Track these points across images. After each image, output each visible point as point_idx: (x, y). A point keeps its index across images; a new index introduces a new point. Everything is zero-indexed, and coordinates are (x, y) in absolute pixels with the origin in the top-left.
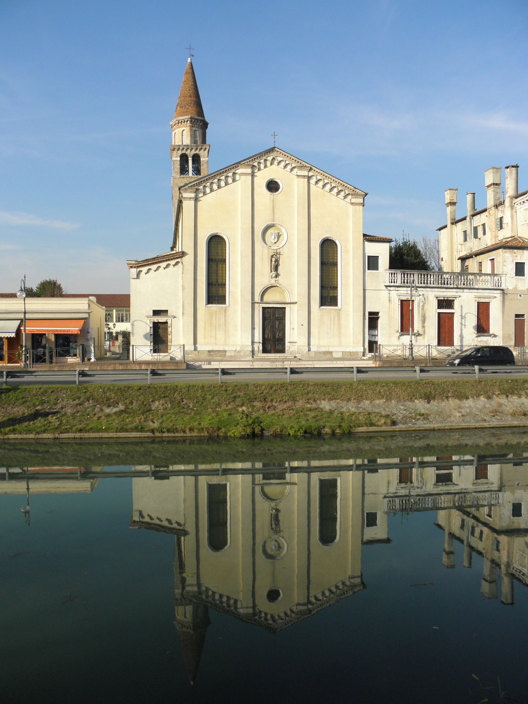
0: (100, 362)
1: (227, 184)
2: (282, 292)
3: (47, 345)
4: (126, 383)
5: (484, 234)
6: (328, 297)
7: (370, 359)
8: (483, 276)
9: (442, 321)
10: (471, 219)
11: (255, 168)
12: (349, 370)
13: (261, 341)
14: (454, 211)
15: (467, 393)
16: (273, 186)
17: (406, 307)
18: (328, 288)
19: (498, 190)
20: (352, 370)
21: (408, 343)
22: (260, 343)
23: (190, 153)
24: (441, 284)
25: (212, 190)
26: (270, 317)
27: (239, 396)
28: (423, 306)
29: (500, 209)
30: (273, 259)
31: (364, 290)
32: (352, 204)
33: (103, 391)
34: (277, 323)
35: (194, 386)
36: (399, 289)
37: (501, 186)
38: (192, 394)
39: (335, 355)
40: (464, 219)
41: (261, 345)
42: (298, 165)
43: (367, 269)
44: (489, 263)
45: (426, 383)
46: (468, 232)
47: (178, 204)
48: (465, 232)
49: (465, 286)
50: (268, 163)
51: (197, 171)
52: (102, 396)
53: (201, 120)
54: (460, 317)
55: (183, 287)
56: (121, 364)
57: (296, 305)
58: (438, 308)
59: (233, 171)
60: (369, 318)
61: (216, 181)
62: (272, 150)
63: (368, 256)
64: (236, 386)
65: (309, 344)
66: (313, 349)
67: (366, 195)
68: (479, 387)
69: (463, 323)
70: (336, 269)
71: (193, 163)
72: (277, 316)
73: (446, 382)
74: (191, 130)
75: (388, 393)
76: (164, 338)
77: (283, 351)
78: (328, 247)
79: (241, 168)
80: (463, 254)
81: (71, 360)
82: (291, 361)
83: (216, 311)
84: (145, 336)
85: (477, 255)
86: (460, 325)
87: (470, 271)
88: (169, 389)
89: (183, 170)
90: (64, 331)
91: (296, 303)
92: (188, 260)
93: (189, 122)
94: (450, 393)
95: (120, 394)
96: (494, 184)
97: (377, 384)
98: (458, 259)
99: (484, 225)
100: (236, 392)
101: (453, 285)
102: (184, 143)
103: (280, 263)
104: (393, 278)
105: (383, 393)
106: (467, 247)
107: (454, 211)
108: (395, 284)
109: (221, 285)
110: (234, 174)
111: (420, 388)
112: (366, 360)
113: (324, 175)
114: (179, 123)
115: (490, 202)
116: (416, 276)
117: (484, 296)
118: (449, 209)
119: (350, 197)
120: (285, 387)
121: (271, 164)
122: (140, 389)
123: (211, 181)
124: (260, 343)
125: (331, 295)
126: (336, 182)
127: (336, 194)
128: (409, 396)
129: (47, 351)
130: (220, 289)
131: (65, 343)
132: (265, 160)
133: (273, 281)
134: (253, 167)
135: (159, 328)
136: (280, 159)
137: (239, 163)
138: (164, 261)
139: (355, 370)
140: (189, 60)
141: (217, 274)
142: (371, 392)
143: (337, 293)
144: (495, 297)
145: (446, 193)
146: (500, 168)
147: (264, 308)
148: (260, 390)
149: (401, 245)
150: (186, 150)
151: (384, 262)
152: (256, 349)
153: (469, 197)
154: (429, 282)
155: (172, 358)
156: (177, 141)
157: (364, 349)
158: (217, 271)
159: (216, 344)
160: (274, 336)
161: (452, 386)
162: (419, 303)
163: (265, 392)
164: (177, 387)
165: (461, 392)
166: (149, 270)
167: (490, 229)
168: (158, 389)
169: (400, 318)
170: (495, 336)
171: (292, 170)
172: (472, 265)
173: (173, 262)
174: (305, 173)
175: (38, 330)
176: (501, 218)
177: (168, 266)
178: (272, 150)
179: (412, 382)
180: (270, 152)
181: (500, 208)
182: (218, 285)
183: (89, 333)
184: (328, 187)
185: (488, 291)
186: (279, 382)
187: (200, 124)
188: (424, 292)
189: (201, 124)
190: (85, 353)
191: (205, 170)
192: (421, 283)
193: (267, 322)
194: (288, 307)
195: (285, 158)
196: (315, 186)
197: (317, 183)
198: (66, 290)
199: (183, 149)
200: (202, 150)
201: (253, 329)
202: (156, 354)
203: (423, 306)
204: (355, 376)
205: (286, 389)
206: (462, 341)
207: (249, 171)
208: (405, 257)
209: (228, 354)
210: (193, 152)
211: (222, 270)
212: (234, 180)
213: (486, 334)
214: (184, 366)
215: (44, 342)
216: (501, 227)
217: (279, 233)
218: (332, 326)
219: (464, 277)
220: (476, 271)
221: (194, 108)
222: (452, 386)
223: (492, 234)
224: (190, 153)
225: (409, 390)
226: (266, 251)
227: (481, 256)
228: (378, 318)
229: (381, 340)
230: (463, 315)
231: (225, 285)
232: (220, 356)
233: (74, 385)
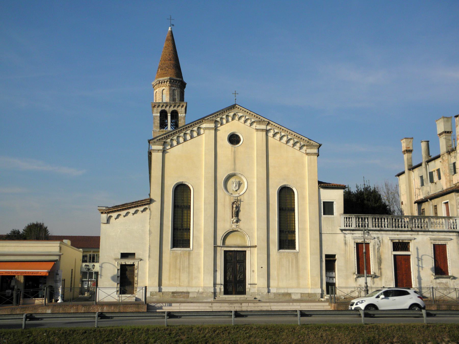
0: (66, 303)
1: (192, 137)
2: (243, 237)
3: (16, 287)
4: (74, 327)
5: (440, 178)
6: (287, 241)
7: (327, 301)
8: (440, 219)
9: (399, 263)
10: (426, 165)
11: (218, 123)
12: (293, 313)
13: (223, 283)
14: (411, 158)
15: (414, 339)
16: (234, 139)
17: (362, 251)
18: (286, 232)
19: (450, 138)
20: (296, 313)
21: (363, 285)
22: (221, 284)
23: (169, 110)
24: (396, 227)
25: (178, 143)
26: (232, 260)
27: (182, 340)
28: (379, 249)
29: (453, 155)
30: (234, 206)
31: (321, 234)
32: (307, 154)
33: (48, 335)
34: (238, 266)
35: (139, 329)
36: (354, 232)
37: (453, 134)
38: (136, 337)
39: (294, 297)
40: (420, 165)
41: (222, 287)
42: (257, 119)
44: (444, 207)
45: (370, 328)
46: (424, 177)
47: (148, 156)
48: (422, 177)
49: (420, 229)
50: (230, 119)
51: (175, 125)
52: (44, 341)
53: (179, 81)
54: (416, 259)
55: (150, 231)
56: (83, 306)
57: (256, 249)
58: (394, 250)
59: (198, 126)
60: (326, 261)
61: (182, 134)
62: (233, 107)
63: (324, 202)
64: (180, 329)
65: (268, 286)
66: (273, 290)
67: (320, 145)
68: (426, 333)
69: (420, 265)
70: (293, 214)
71: (171, 119)
72: (238, 259)
73: (391, 326)
74: (170, 90)
75: (330, 337)
76: (131, 280)
77: (243, 292)
78: (286, 194)
79: (205, 123)
80: (421, 197)
81: (38, 301)
82: (249, 303)
83: (181, 254)
84: (113, 278)
85: (432, 198)
86: (417, 267)
87: (427, 214)
88: (113, 332)
89: (163, 125)
90: (33, 273)
91: (256, 246)
92: (156, 206)
93: (168, 82)
94: (396, 338)
95: (63, 338)
96: (445, 132)
97: (320, 327)
98: (415, 203)
99: (438, 170)
100: (179, 336)
101: (408, 227)
102: (164, 101)
103: (241, 209)
104: (348, 222)
105: (325, 338)
106: (424, 192)
107: (411, 158)
108: (350, 228)
109: (186, 229)
110: (199, 128)
111: (363, 332)
112: (324, 302)
113: (280, 129)
114: (159, 83)
115: (443, 149)
116: (370, 220)
117: (440, 238)
118: (406, 156)
119: (305, 148)
120: (228, 331)
121: (233, 119)
122: (85, 332)
123: (177, 135)
124: (221, 284)
125: (289, 238)
126: (292, 134)
127: (292, 146)
128: (351, 341)
129: (14, 293)
130: (185, 233)
131: (34, 285)
132: (227, 116)
133: (234, 226)
134: (216, 122)
135: (126, 270)
136: (240, 114)
137: (203, 118)
138: (133, 207)
139: (298, 313)
140: (170, 29)
141: (182, 219)
142: (313, 336)
143: (295, 237)
144: (451, 239)
145: (402, 141)
146: (451, 118)
147: (225, 252)
148: (203, 333)
149: (362, 190)
150: (166, 107)
151: (339, 207)
152: (218, 290)
153: (423, 145)
154: (383, 225)
155: (137, 299)
156: (157, 99)
157: (322, 291)
158: (182, 216)
159: (180, 286)
160: (235, 277)
161: (397, 331)
162: (374, 246)
163: (207, 336)
164: (122, 330)
165: (407, 338)
166: (119, 215)
167: (444, 174)
168: (103, 332)
169: (356, 261)
170: (454, 278)
171: (251, 124)
172: (428, 208)
173: (141, 208)
174: (264, 127)
175: (6, 272)
176: (454, 164)
177: (136, 212)
178: (233, 107)
179: (355, 326)
180: (231, 108)
181: (452, 154)
182: (183, 230)
183: (58, 274)
184: (285, 139)
185: (443, 234)
186: (224, 325)
187: (178, 85)
188: (379, 235)
190: (52, 295)
191: (181, 123)
192: (376, 227)
193: (229, 264)
195: (245, 114)
196: (272, 139)
197: (274, 135)
198: (52, 232)
199: (163, 106)
200: (180, 107)
201: (215, 271)
202: (123, 295)
203: (379, 249)
204: (299, 320)
205: (229, 333)
206: (420, 283)
207: (213, 125)
208: (366, 202)
209: (191, 295)
210: (172, 109)
211: (187, 216)
212: (199, 134)
213: (444, 276)
214: (144, 309)
215: (13, 283)
216: (455, 172)
217: (239, 182)
219: (420, 221)
220: (432, 214)
221: (173, 70)
222: (397, 331)
223: (446, 179)
224: (169, 110)
225: (352, 334)
226: (227, 198)
227: (436, 200)
228: (335, 260)
229: (338, 281)
230: (420, 257)
231: (189, 229)
232: (183, 297)
233: (20, 330)
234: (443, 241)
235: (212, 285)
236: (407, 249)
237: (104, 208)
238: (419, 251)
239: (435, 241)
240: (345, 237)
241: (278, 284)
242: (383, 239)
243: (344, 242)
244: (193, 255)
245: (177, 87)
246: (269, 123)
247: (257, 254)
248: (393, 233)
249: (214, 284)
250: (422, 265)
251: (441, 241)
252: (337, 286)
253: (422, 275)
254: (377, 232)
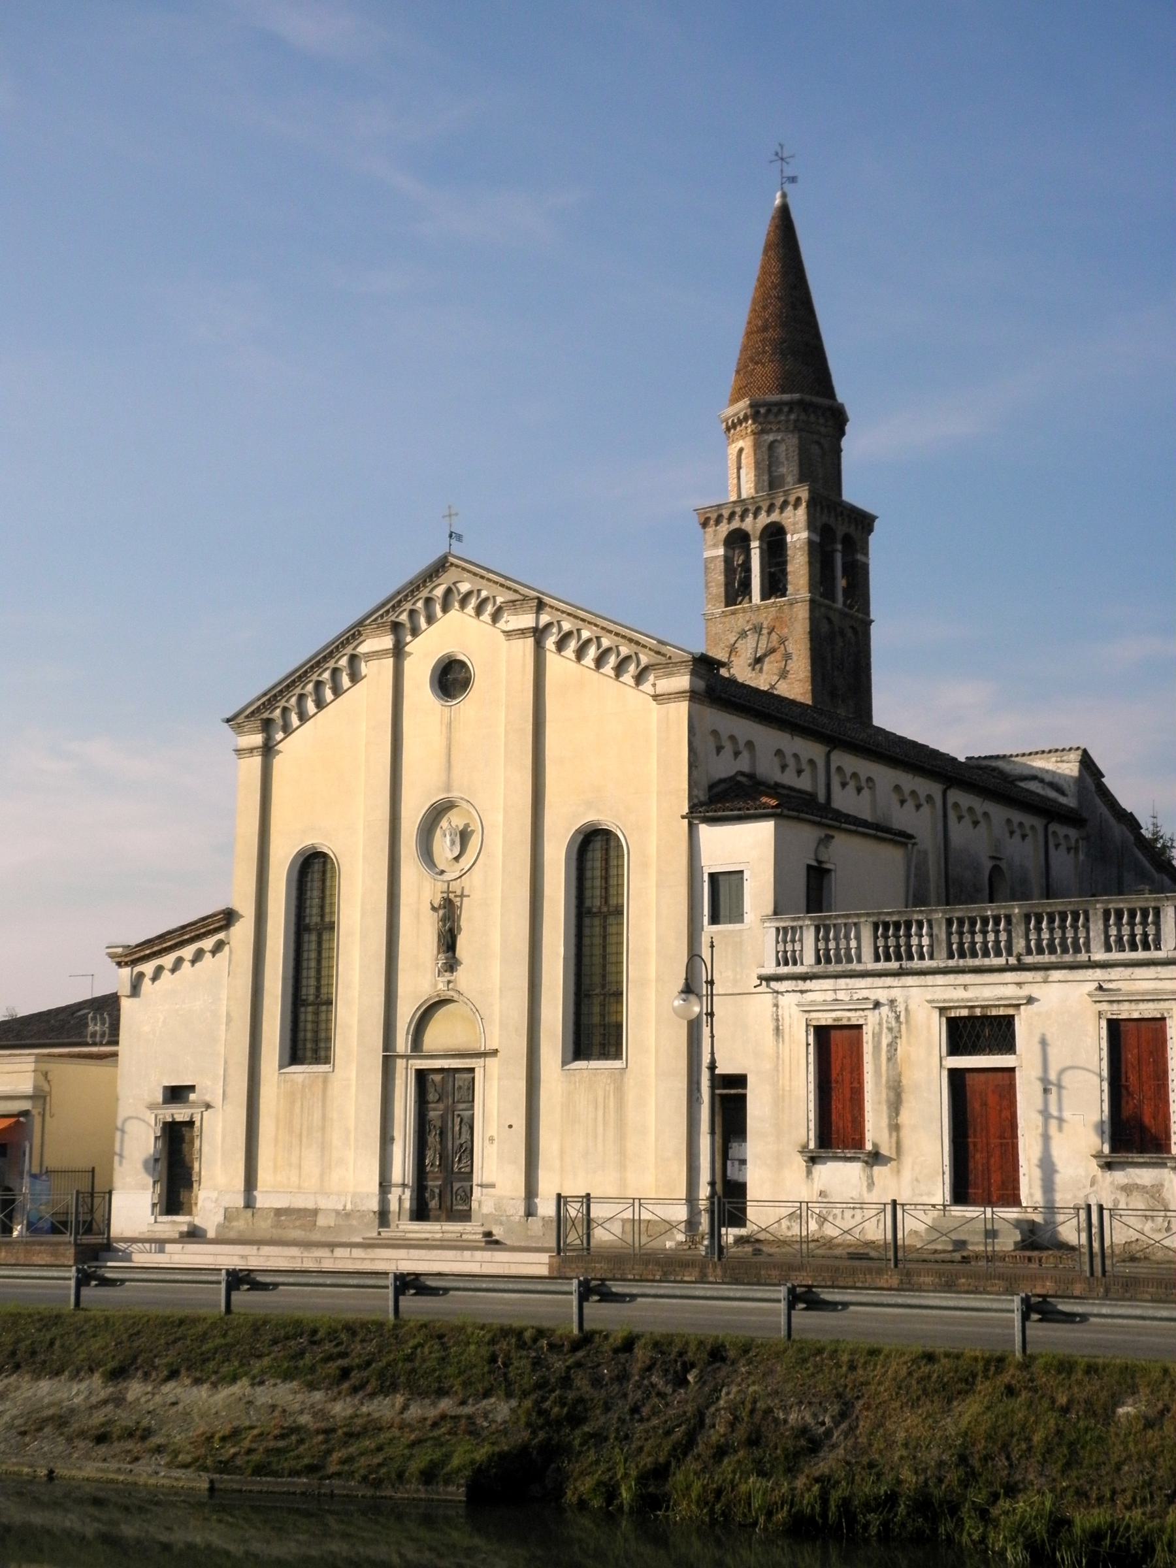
6: (595, 1031)
9: (974, 1106)
13: (409, 1180)
17: (835, 1055)
23: (753, 525)
24: (922, 957)
28: (893, 1046)
36: (809, 985)
41: (408, 1193)
43: (706, 920)
55: (228, 1014)
69: (1054, 1111)
77: (465, 1216)
78: (596, 850)
79: (368, 637)
89: (736, 591)
91: (495, 1053)
92: (241, 933)
108: (799, 969)
110: (353, 658)
136: (464, 587)
137: (361, 623)
147: (421, 1075)
150: (742, 520)
151: (758, 893)
152: (394, 1206)
162: (877, 1036)
177: (198, 956)
180: (437, 571)
189: (793, 417)
197: (561, 645)
200: (790, 508)
201: (386, 1140)
203: (893, 1046)
206: (1048, 1186)
209: (321, 1221)
210: (764, 520)
212: (355, 678)
218: (600, 1130)
224: (753, 525)
229: (759, 1180)
230: (1053, 1076)
234: (1151, 1005)
235: (375, 1188)
236: (1007, 1044)
237: (120, 950)
238: (1052, 1052)
239: (1115, 1007)
240: (776, 1005)
241: (561, 1186)
242: (912, 1007)
243: (771, 1026)
244: (630, 1080)
245: (787, 430)
246: (540, 606)
247: (499, 1079)
248: (951, 979)
249: (381, 1184)
250: (1060, 1109)
251: (1142, 1006)
252: (751, 1194)
253: (1059, 1153)
254: (889, 981)
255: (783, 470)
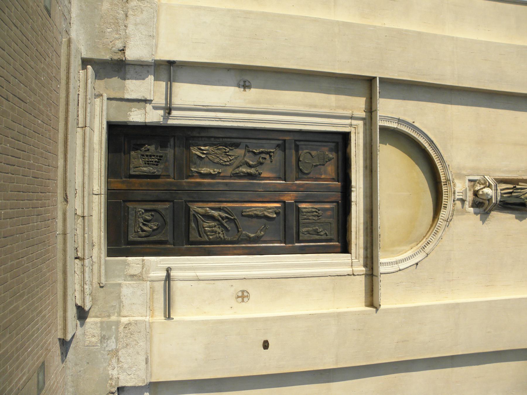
2: (408, 239)
13: (178, 119)
22: (168, 110)
41: (154, 117)
57: (356, 304)
77: (122, 241)
124: (168, 110)
152: (135, 88)
194: (350, 263)
201: (245, 76)
235: (165, 54)
249: (171, 63)
255: (71, 390)
